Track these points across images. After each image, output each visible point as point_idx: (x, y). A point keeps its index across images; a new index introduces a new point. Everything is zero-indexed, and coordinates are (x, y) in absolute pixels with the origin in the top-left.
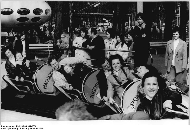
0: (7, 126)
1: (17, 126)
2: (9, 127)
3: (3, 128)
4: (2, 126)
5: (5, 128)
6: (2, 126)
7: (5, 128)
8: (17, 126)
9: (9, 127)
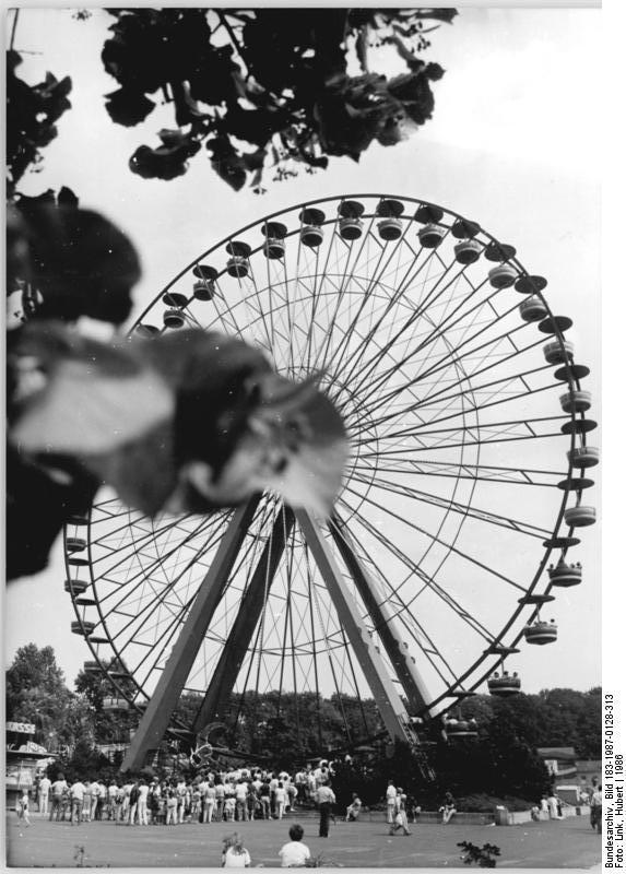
0: (610, 844)
3: (615, 859)
5: (615, 853)
7: (615, 853)
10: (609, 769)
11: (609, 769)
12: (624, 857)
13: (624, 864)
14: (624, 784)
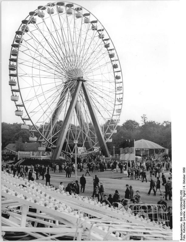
0: (181, 234)
1: (181, 221)
2: (182, 230)
3: (183, 238)
4: (181, 240)
5: (183, 236)
6: (181, 240)
7: (183, 236)
8: (181, 221)
9: (182, 230)
10: (181, 213)
11: (181, 213)
12: (185, 237)
13: (185, 239)
14: (185, 190)
